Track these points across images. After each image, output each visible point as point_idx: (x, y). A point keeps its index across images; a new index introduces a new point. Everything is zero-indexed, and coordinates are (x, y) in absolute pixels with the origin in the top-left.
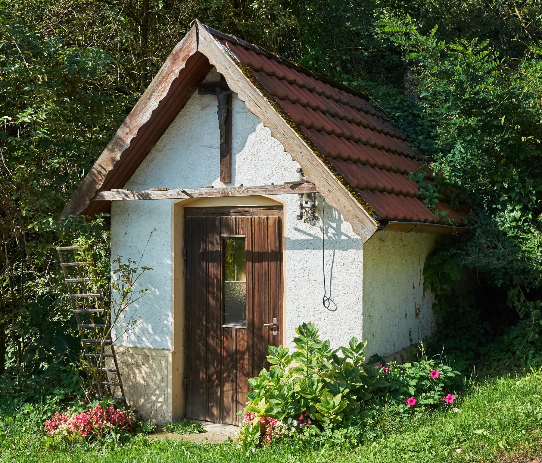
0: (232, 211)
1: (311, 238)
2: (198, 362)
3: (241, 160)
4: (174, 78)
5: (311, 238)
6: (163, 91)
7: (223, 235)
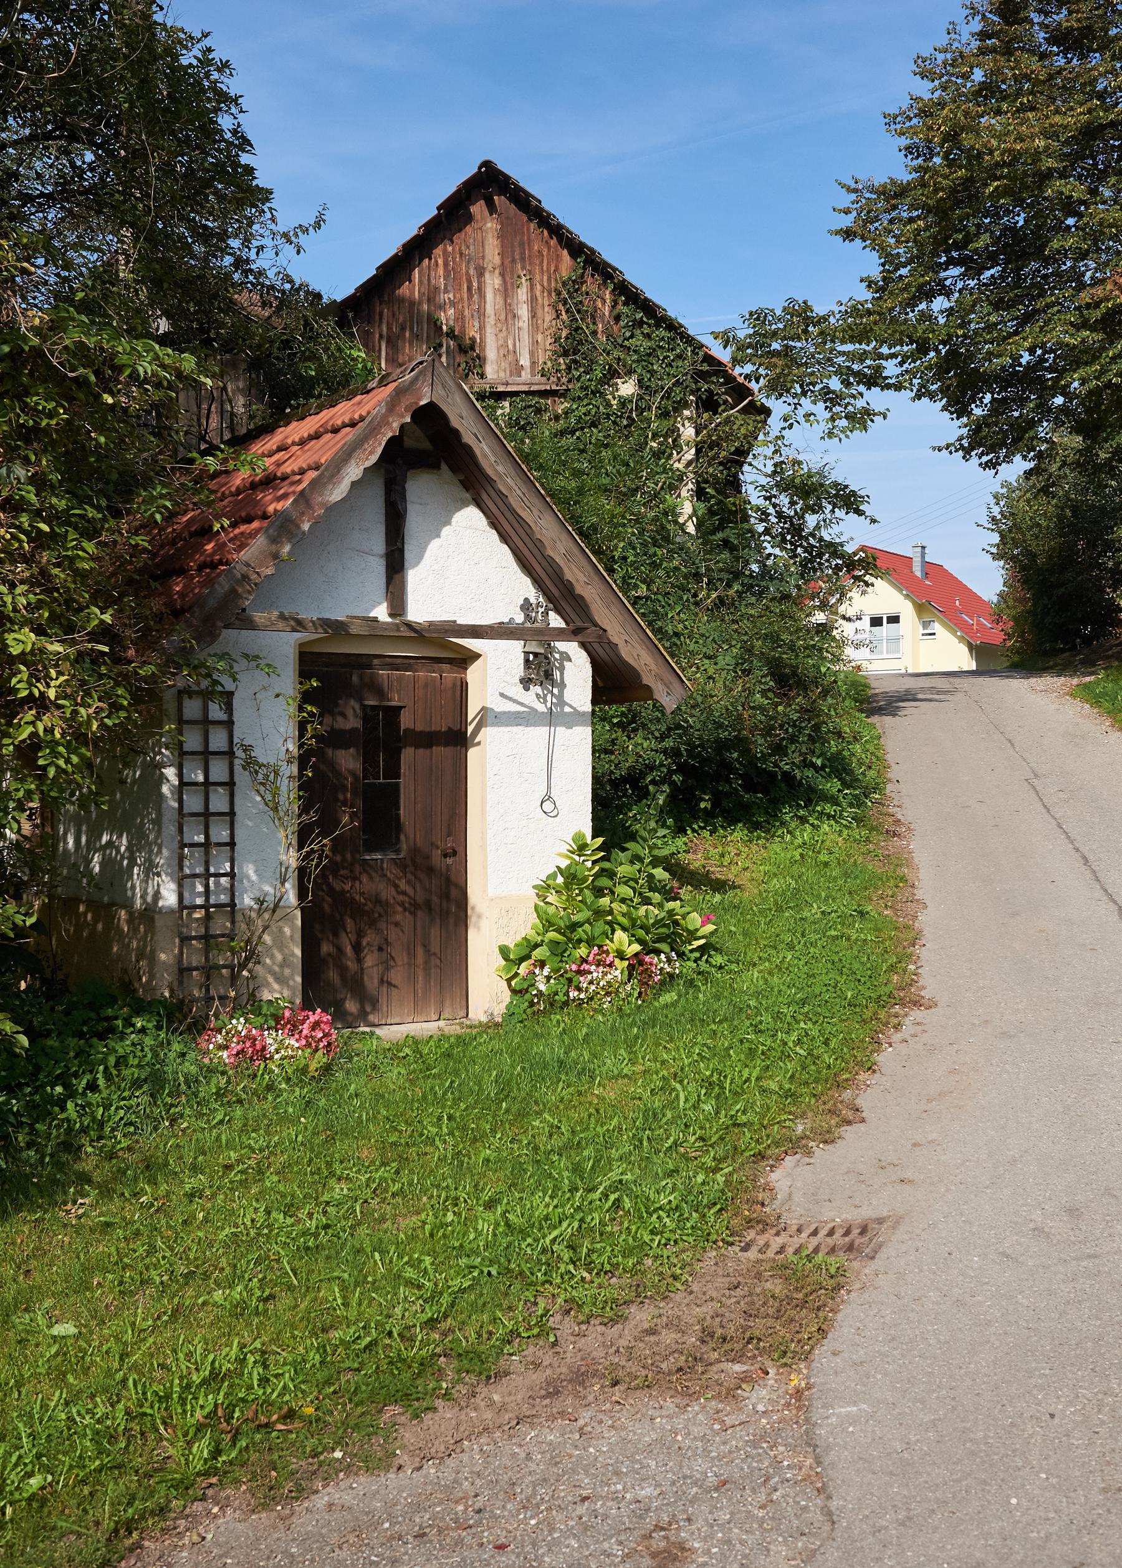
0: (376, 661)
1: (523, 709)
2: (317, 926)
3: (415, 578)
4: (390, 434)
5: (523, 709)
6: (371, 453)
7: (366, 703)
